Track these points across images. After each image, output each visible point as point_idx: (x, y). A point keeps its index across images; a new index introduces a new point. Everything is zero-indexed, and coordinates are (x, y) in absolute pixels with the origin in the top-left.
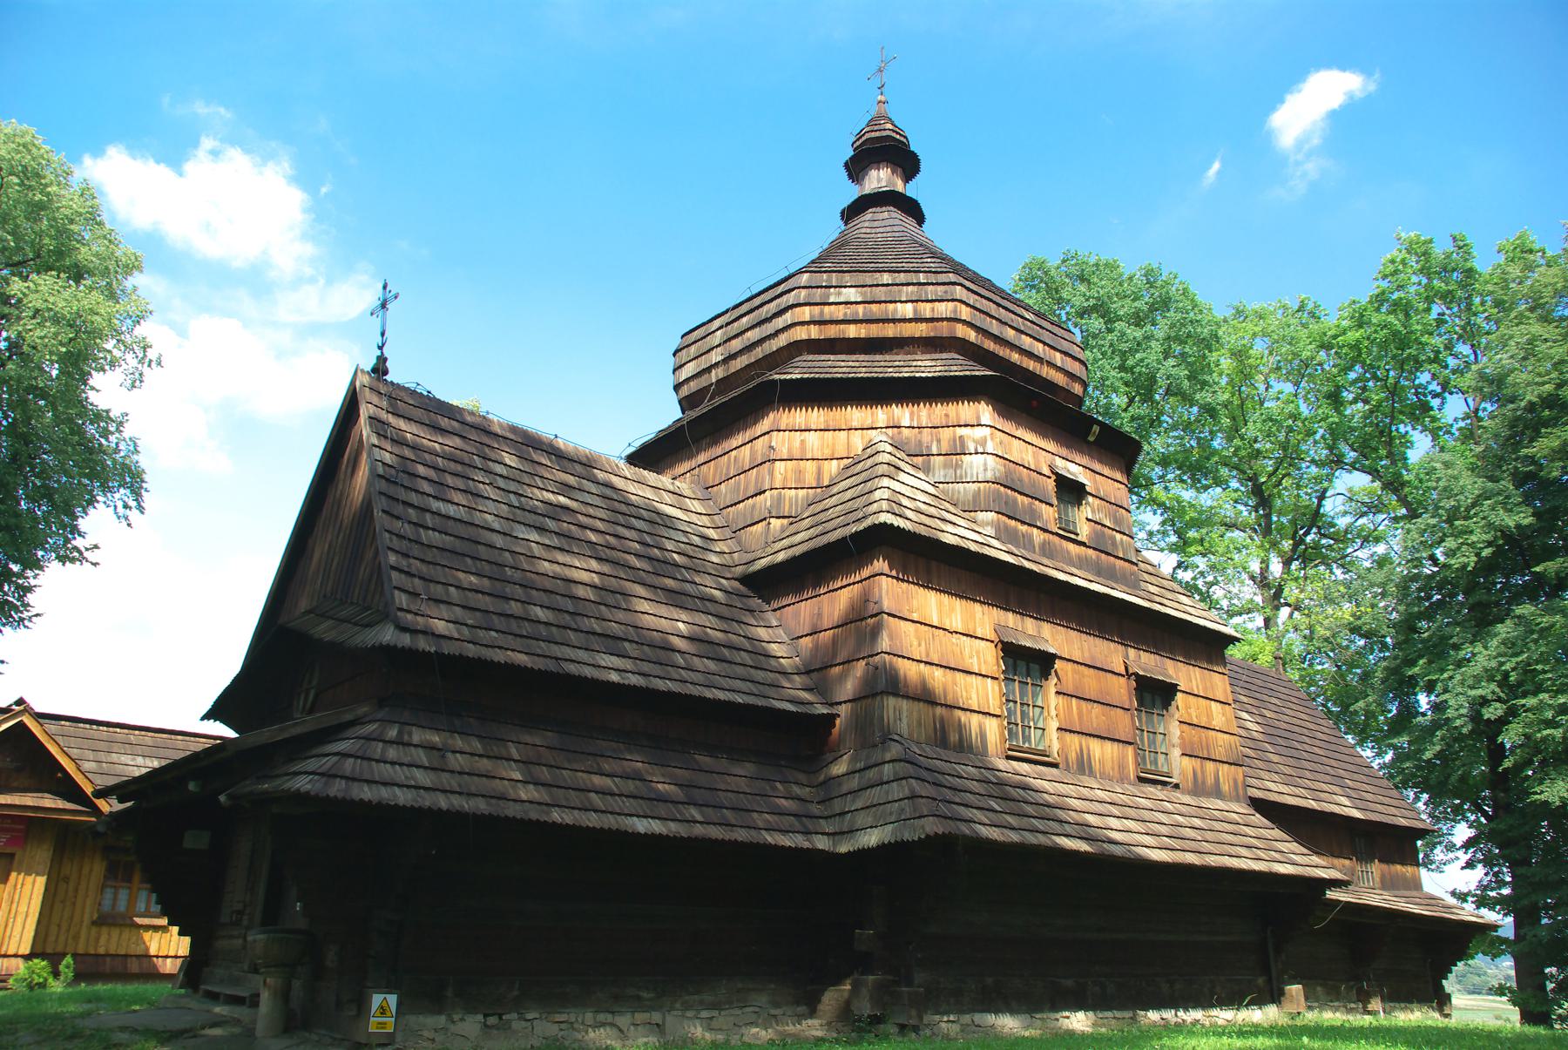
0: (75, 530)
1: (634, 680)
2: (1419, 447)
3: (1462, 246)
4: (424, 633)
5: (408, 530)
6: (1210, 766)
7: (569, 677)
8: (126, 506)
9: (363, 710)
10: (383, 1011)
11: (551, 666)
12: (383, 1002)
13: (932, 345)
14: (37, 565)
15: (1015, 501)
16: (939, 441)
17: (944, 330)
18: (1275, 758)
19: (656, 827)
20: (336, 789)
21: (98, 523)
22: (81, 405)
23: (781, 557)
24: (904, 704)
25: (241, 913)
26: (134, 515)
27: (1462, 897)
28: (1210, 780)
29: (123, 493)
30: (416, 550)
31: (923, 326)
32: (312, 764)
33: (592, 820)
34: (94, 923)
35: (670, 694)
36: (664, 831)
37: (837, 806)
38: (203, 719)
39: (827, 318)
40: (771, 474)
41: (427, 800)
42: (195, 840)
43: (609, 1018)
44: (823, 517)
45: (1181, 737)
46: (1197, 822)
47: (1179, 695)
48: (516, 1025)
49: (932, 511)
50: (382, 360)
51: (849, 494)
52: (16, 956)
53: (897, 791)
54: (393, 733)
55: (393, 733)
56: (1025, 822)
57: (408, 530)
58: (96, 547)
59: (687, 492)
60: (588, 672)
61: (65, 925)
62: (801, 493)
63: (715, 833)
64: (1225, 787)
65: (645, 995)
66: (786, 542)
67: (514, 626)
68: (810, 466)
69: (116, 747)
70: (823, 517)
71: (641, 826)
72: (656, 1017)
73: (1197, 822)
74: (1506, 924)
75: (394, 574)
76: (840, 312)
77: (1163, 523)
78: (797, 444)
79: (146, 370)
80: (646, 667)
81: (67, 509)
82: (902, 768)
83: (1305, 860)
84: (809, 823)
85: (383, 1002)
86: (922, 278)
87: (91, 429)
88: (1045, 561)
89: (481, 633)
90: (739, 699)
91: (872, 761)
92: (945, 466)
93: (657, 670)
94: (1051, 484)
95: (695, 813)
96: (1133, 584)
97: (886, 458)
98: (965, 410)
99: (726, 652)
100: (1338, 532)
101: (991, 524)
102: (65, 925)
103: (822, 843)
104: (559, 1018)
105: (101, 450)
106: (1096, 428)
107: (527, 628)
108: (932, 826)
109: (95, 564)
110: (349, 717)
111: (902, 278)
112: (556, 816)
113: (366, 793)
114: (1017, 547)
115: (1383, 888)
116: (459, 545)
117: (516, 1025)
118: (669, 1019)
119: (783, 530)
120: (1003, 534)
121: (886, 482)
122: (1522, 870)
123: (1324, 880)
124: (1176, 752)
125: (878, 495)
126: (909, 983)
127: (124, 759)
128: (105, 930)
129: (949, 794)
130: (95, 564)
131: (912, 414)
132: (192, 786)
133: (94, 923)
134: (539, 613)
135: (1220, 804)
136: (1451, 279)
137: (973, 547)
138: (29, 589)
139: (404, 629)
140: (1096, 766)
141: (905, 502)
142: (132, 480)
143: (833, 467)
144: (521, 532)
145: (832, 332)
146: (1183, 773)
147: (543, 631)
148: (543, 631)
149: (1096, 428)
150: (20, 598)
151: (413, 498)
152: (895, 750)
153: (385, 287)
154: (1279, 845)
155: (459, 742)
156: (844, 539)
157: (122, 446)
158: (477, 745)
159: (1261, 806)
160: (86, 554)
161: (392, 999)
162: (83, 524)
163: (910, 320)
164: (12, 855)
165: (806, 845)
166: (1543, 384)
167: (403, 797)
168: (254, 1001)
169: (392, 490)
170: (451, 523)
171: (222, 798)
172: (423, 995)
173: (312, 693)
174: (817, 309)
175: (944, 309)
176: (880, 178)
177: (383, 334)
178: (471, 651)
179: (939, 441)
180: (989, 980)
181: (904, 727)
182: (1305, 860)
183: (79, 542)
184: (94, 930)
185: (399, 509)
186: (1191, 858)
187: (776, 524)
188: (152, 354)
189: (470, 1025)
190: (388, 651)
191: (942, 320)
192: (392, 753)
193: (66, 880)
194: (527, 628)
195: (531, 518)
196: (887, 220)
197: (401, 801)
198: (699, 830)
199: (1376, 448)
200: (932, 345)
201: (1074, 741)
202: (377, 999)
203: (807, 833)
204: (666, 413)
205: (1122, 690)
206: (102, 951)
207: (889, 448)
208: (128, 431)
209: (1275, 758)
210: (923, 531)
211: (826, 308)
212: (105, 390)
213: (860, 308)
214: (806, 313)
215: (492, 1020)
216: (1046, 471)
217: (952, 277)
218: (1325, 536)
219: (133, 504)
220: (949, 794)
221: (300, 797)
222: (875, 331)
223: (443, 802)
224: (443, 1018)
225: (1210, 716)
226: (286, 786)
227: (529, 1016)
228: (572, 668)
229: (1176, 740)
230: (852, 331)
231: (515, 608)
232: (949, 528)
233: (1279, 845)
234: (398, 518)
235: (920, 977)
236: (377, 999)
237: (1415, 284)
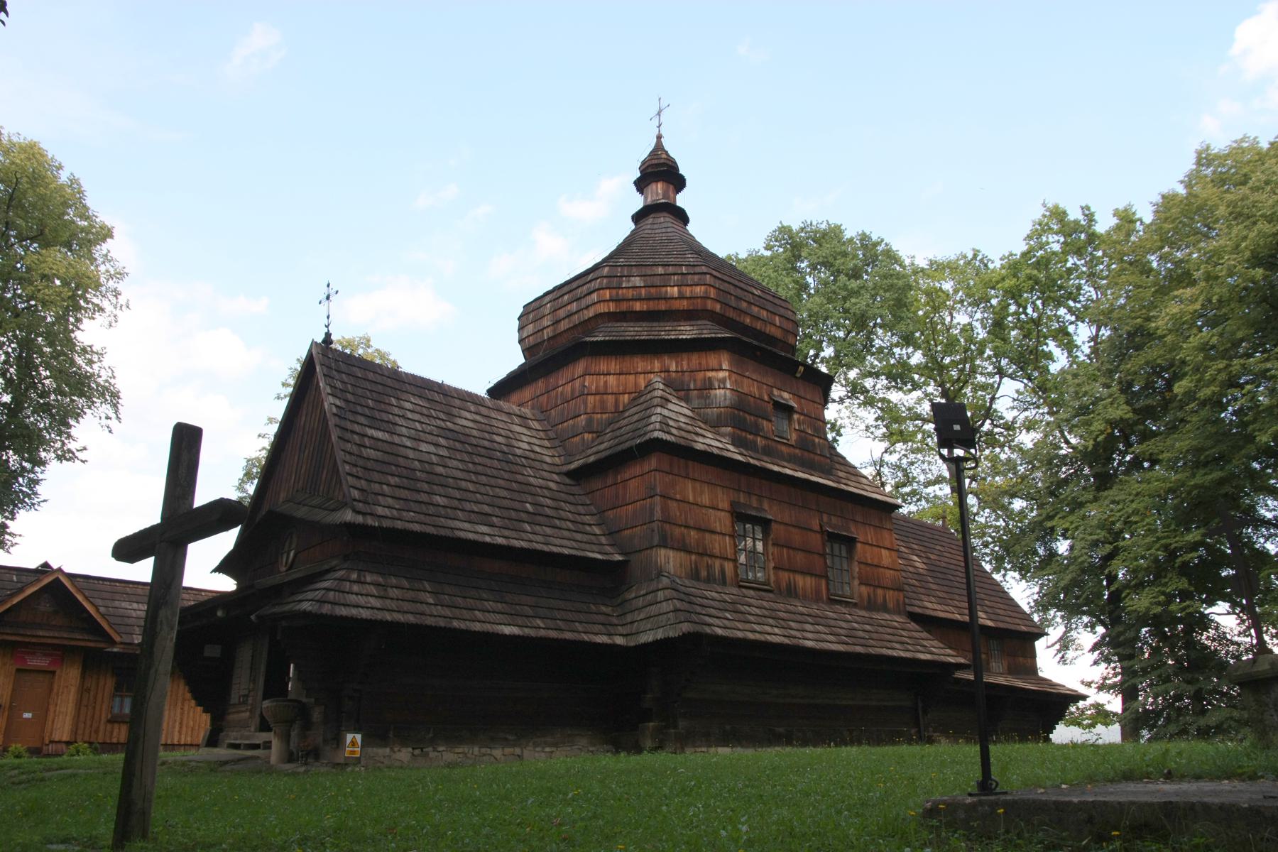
0: (69, 436)
1: (500, 541)
2: (1059, 362)
3: (1090, 218)
4: (371, 514)
5: (355, 449)
6: (880, 591)
7: (459, 540)
8: (108, 418)
9: (334, 563)
10: (353, 743)
11: (448, 533)
12: (353, 739)
14: (42, 463)
15: (745, 419)
17: (699, 304)
18: (934, 587)
19: (515, 630)
20: (326, 609)
21: (87, 430)
22: (71, 343)
23: (592, 459)
25: (247, 696)
26: (113, 423)
27: (1089, 685)
28: (880, 600)
29: (106, 409)
30: (361, 462)
31: (685, 302)
32: (310, 595)
33: (477, 627)
34: (109, 721)
35: (522, 549)
36: (521, 633)
37: (629, 618)
38: (215, 570)
40: (585, 403)
41: (379, 616)
42: (213, 651)
43: (488, 751)
44: (618, 433)
45: (860, 573)
46: (868, 627)
47: (859, 545)
48: (432, 754)
49: (690, 428)
50: (328, 335)
51: (636, 418)
52: (60, 742)
53: (665, 607)
54: (354, 576)
55: (354, 576)
56: (748, 626)
57: (355, 449)
58: (85, 449)
59: (529, 415)
60: (471, 536)
61: (88, 723)
62: (605, 416)
63: (553, 634)
64: (891, 605)
65: (510, 737)
66: (594, 449)
67: (424, 508)
68: (611, 399)
69: (117, 596)
70: (618, 433)
71: (507, 630)
72: (518, 751)
73: (868, 627)
74: (1114, 703)
75: (349, 478)
76: (630, 294)
77: (877, 419)
79: (118, 312)
80: (507, 533)
81: (63, 419)
82: (668, 593)
83: (942, 651)
84: (611, 629)
85: (353, 739)
86: (684, 270)
87: (79, 361)
88: (765, 458)
89: (405, 514)
90: (566, 551)
91: (651, 589)
92: (699, 397)
93: (513, 534)
94: (770, 407)
95: (539, 622)
96: (827, 472)
97: (659, 393)
98: (712, 360)
99: (557, 522)
100: (1006, 423)
101: (729, 435)
102: (88, 723)
103: (619, 641)
104: (457, 750)
105: (90, 377)
106: (801, 369)
107: (432, 510)
108: (686, 627)
109: (83, 462)
110: (326, 567)
111: (671, 270)
112: (455, 624)
113: (344, 612)
114: (747, 449)
115: (1010, 673)
116: (386, 458)
117: (432, 754)
118: (526, 753)
119: (593, 440)
120: (737, 442)
121: (659, 410)
122: (1126, 664)
123: (951, 664)
124: (856, 582)
125: (653, 419)
126: (676, 727)
127: (124, 605)
128: (116, 726)
129: (699, 609)
130: (83, 462)
132: (220, 613)
133: (109, 721)
134: (439, 500)
135: (887, 616)
136: (1079, 236)
137: (716, 451)
138: (37, 482)
139: (359, 513)
140: (801, 592)
141: (671, 423)
142: (111, 396)
144: (424, 447)
145: (624, 307)
146: (860, 596)
147: (443, 511)
148: (443, 511)
149: (801, 369)
150: (31, 489)
151: (357, 428)
152: (665, 581)
154: (925, 643)
155: (394, 581)
156: (631, 448)
157: (103, 373)
158: (405, 583)
159: (914, 617)
160: (77, 454)
161: (359, 737)
162: (73, 431)
164: (54, 673)
165: (609, 641)
166: (1135, 318)
167: (365, 614)
168: (267, 745)
169: (343, 423)
170: (380, 443)
171: (253, 617)
172: (375, 736)
173: (292, 554)
174: (614, 292)
175: (699, 290)
176: (658, 190)
178: (399, 525)
180: (728, 727)
181: (671, 567)
182: (942, 651)
183: (72, 445)
184: (109, 726)
185: (348, 436)
186: (859, 649)
187: (588, 436)
188: (122, 300)
189: (404, 754)
190: (349, 526)
192: (356, 588)
193: (88, 690)
194: (432, 510)
195: (430, 438)
196: (664, 219)
197: (364, 616)
198: (542, 633)
199: (1028, 361)
200: (689, 315)
201: (785, 576)
202: (349, 737)
203: (610, 635)
204: (514, 359)
205: (815, 540)
206: (115, 740)
207: (661, 386)
208: (107, 362)
209: (934, 587)
210: (682, 442)
212: (88, 333)
213: (643, 291)
214: (607, 294)
215: (417, 752)
216: (766, 398)
217: (704, 269)
218: (997, 426)
219: (114, 416)
220: (699, 609)
221: (306, 614)
222: (652, 306)
223: (388, 617)
224: (388, 750)
225: (880, 557)
226: (297, 608)
227: (441, 749)
228: (462, 535)
229: (856, 575)
230: (638, 306)
231: (424, 497)
232: (701, 439)
233: (925, 643)
235: (682, 724)
236: (349, 737)
237: (1055, 243)
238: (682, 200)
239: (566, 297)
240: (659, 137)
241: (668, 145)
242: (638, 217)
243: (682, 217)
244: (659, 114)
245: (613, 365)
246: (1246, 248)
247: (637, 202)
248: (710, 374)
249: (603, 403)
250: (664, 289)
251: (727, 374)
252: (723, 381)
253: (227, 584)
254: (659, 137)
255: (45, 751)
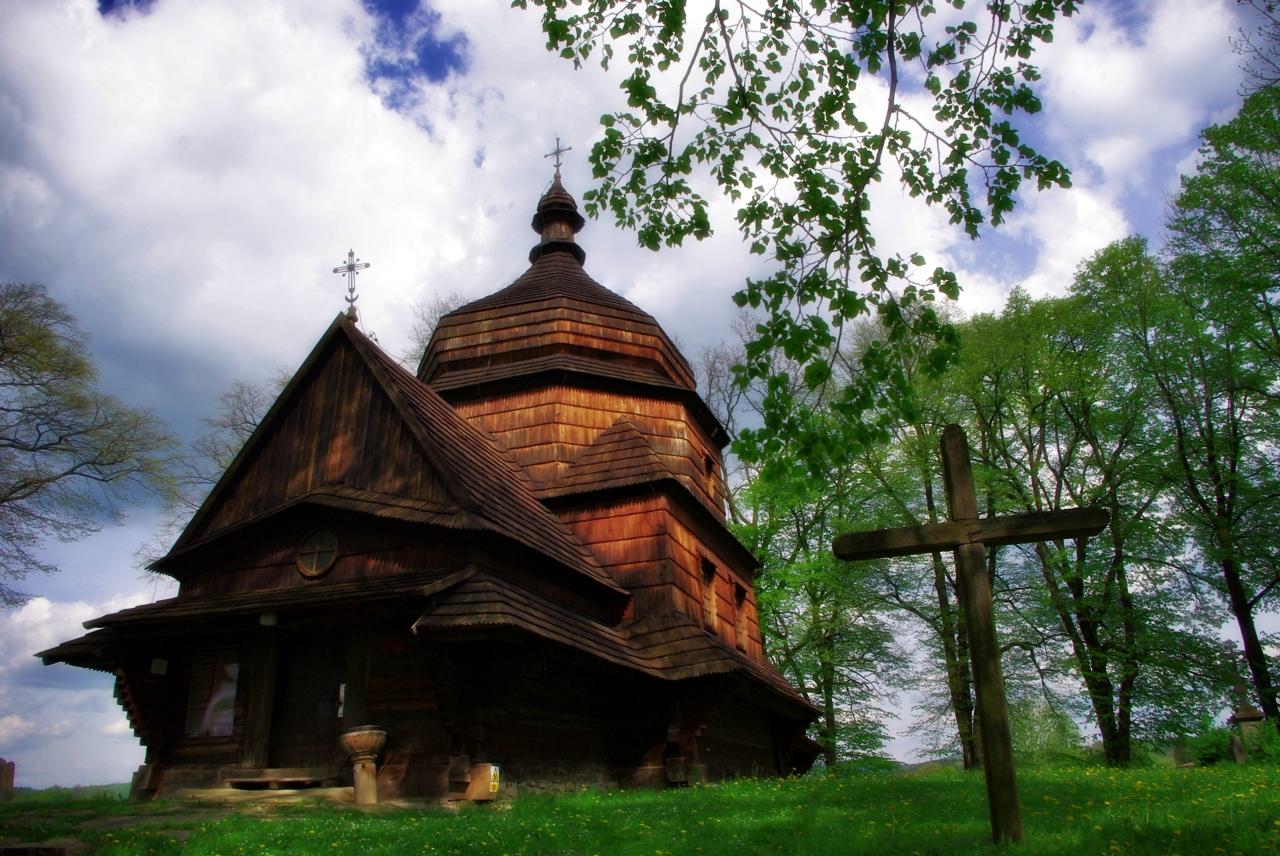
13: (640, 361)
16: (656, 427)
24: (563, 426)
31: (637, 349)
38: (733, 201)
39: (580, 331)
50: (352, 310)
78: (571, 414)
90: (543, 633)
131: (641, 408)
143: (594, 434)
145: (583, 341)
153: (351, 254)
163: (630, 344)
176: (560, 231)
177: (352, 290)
179: (656, 427)
191: (648, 347)
211: (580, 325)
214: (568, 325)
230: (595, 344)
234: (556, 308)
238: (579, 239)
239: (512, 319)
240: (557, 177)
241: (565, 184)
242: (536, 254)
243: (578, 255)
244: (558, 153)
245: (584, 397)
246: (916, 370)
247: (536, 239)
248: (671, 423)
249: (573, 433)
250: (619, 332)
251: (684, 425)
252: (681, 431)
253: (167, 588)
254: (557, 177)
255: (1272, 22)
